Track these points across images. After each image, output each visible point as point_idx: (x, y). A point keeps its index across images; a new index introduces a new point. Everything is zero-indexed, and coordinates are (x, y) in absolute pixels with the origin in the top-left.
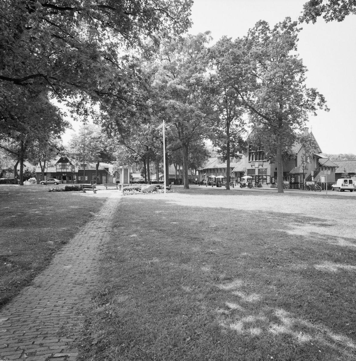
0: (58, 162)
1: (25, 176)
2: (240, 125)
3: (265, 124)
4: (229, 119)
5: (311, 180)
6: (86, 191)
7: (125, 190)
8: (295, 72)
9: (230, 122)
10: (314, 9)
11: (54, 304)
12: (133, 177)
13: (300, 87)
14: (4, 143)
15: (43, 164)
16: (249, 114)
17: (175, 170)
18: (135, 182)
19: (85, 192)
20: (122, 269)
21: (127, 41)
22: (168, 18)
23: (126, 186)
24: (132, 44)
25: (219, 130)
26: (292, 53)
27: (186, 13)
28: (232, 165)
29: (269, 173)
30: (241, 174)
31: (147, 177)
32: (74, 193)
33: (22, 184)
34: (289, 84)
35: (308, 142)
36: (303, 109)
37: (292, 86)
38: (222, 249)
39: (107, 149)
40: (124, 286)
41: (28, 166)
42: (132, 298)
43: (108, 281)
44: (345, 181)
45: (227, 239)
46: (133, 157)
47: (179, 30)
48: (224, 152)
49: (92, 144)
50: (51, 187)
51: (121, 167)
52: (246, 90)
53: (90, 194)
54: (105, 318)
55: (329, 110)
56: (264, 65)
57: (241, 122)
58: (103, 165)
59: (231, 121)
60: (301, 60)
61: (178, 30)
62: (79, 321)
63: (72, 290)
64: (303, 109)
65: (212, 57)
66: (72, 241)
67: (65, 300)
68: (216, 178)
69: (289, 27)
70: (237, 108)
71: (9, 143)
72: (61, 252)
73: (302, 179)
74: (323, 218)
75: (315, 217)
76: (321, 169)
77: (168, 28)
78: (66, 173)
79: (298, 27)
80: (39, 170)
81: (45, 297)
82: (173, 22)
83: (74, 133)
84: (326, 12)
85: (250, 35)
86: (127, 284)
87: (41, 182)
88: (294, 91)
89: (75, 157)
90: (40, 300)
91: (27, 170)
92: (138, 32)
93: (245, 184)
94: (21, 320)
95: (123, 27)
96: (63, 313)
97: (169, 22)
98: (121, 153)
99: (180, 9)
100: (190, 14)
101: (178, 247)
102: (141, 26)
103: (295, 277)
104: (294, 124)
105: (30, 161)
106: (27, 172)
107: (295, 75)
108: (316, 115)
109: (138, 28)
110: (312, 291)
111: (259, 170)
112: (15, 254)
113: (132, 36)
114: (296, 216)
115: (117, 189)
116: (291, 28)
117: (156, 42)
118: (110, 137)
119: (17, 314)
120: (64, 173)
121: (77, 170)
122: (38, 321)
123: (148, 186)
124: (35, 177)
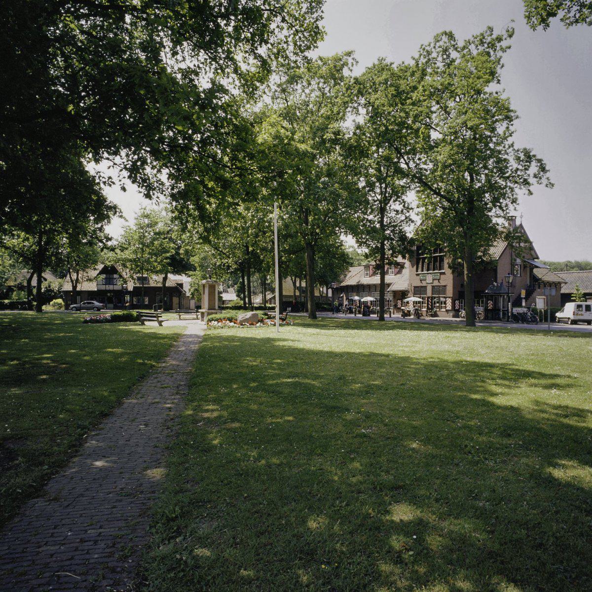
0: (101, 273)
1: (47, 297)
2: (402, 211)
3: (444, 208)
4: (385, 201)
5: (520, 305)
6: (146, 323)
7: (210, 321)
8: (497, 121)
9: (386, 204)
10: (544, 5)
11: (80, 537)
12: (224, 299)
13: (504, 147)
14: (8, 241)
15: (74, 276)
16: (418, 192)
17: (293, 287)
18: (227, 308)
19: (143, 324)
20: (206, 466)
21: (214, 65)
22: (285, 25)
23: (212, 313)
24: (223, 71)
25: (367, 220)
26: (492, 88)
27: (315, 15)
28: (388, 278)
29: (450, 291)
30: (402, 295)
31: (247, 299)
32: (122, 326)
33: (39, 310)
34: (486, 140)
35: (517, 238)
36: (509, 184)
37: (491, 145)
38: (383, 428)
39: (181, 251)
40: (209, 502)
41: (51, 280)
42: (225, 527)
43: (181, 491)
44: (579, 307)
45: (390, 409)
46: (224, 266)
47: (303, 45)
48: (376, 257)
49: (156, 243)
50: (87, 315)
51: (204, 281)
52: (414, 151)
53: (151, 326)
54: (174, 569)
55: (553, 185)
56: (445, 109)
57: (404, 206)
58: (173, 279)
59: (388, 203)
60: (508, 99)
61: (301, 45)
62: (124, 575)
63: (114, 507)
64: (509, 184)
65: (360, 93)
66: (118, 411)
67: (101, 527)
68: (362, 300)
69: (490, 43)
70: (397, 182)
71: (18, 240)
72: (98, 432)
73: (506, 303)
74: (551, 372)
75: (537, 369)
76: (537, 286)
77: (285, 43)
78: (113, 291)
79: (504, 44)
80: (68, 287)
81: (63, 522)
82: (292, 32)
83: (127, 224)
84: (566, 11)
85: (422, 57)
86: (215, 498)
87: (72, 306)
88: (495, 153)
89: (128, 264)
90: (55, 528)
91: (49, 287)
92: (233, 49)
93: (409, 312)
94: (15, 570)
95: (209, 40)
96: (96, 556)
97: (285, 32)
98: (205, 259)
99: (304, 10)
100: (322, 18)
101: (305, 423)
102: (238, 39)
103: (521, 484)
104: (494, 210)
105: (54, 272)
106: (49, 290)
107: (498, 125)
108: (530, 193)
109: (233, 41)
110: (557, 512)
111: (433, 287)
112: (17, 435)
113: (223, 56)
114: (502, 367)
115: (197, 319)
116: (492, 45)
117: (264, 64)
118: (184, 229)
119: (11, 556)
120: (110, 291)
121: (130, 286)
122: (47, 574)
123: (249, 314)
124: (61, 297)
